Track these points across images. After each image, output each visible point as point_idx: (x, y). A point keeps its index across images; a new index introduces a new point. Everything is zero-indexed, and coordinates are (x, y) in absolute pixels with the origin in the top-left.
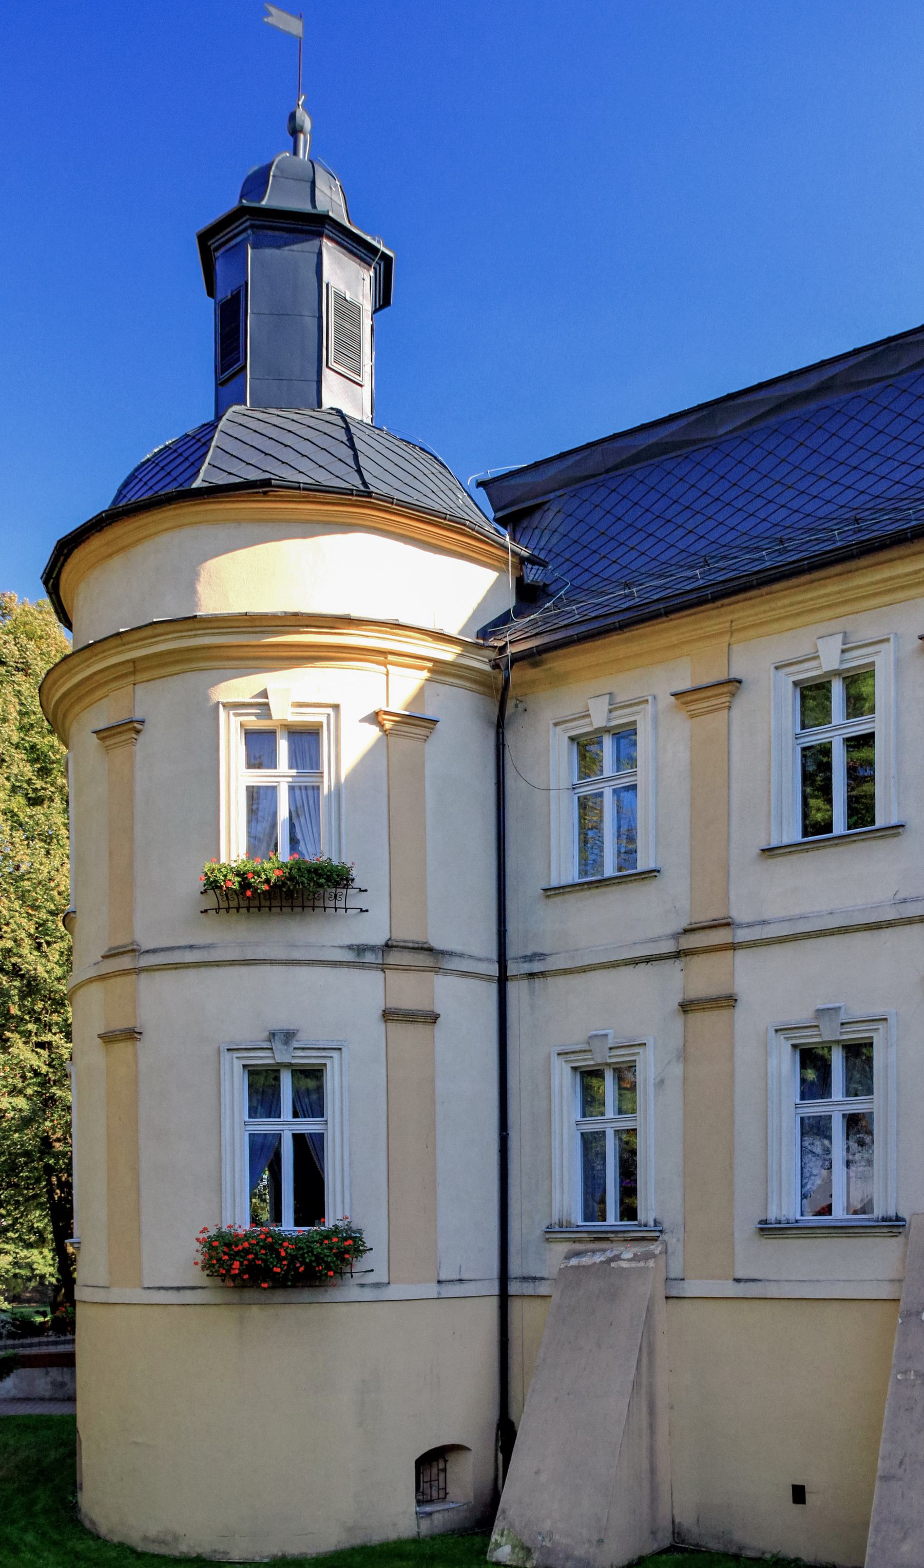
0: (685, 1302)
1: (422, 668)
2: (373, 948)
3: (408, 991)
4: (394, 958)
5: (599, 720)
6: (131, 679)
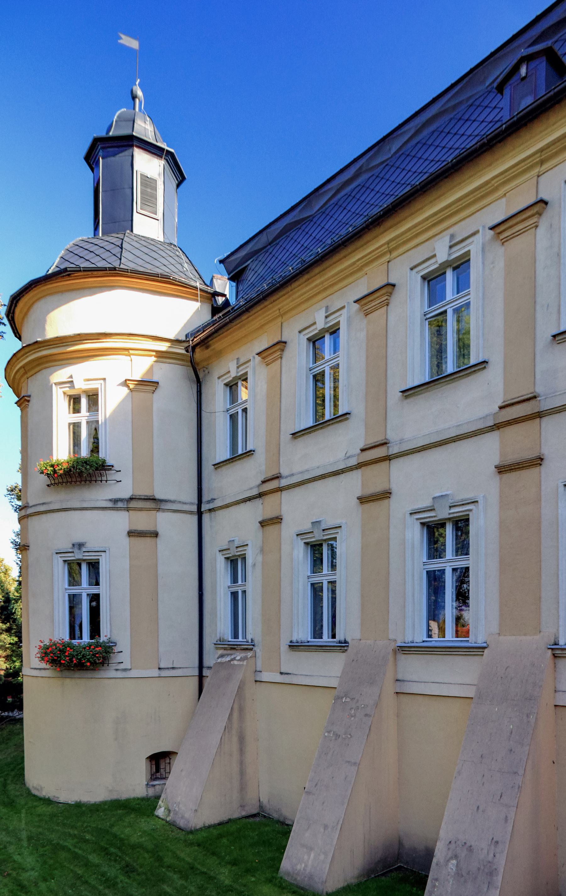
0: (263, 684)
1: (151, 356)
2: (121, 500)
3: (142, 521)
4: (133, 504)
6: (26, 376)
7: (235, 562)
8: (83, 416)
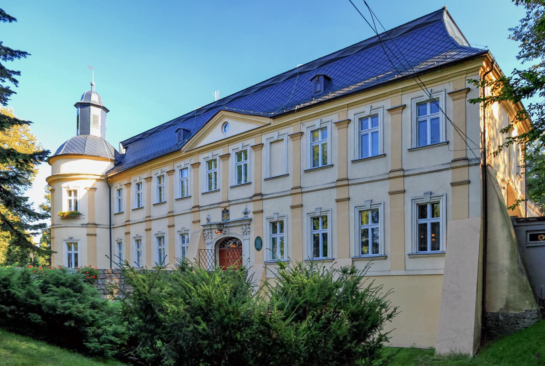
4: (88, 226)
5: (241, 149)
7: (120, 244)
8: (72, 198)
